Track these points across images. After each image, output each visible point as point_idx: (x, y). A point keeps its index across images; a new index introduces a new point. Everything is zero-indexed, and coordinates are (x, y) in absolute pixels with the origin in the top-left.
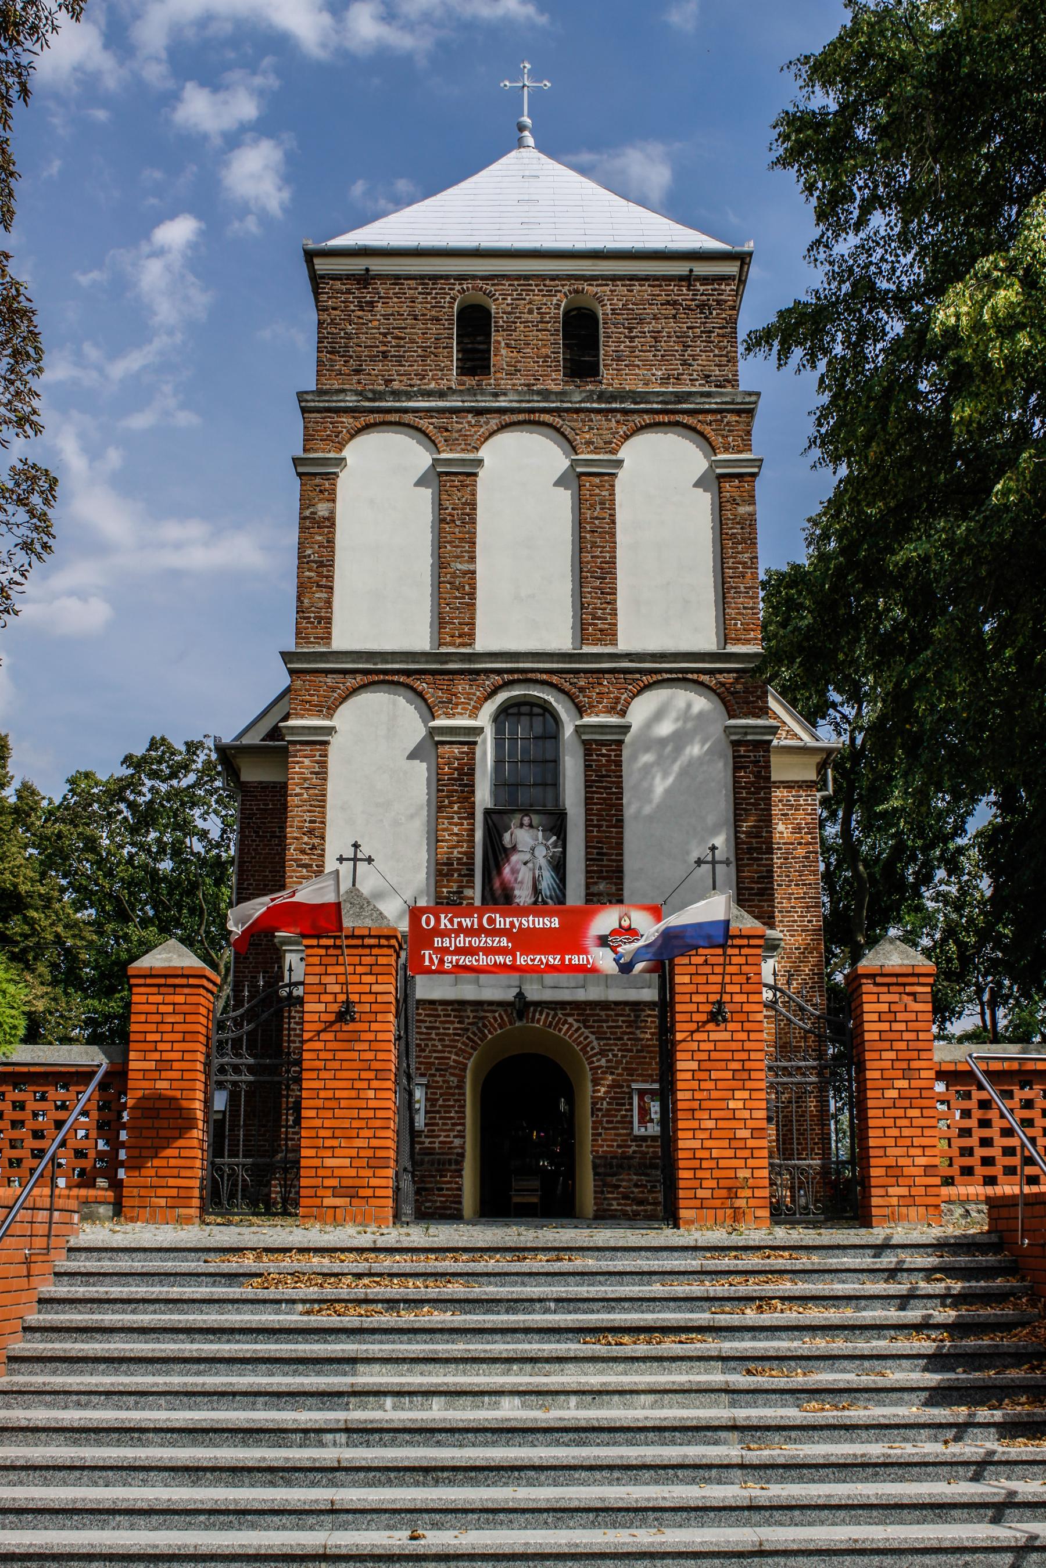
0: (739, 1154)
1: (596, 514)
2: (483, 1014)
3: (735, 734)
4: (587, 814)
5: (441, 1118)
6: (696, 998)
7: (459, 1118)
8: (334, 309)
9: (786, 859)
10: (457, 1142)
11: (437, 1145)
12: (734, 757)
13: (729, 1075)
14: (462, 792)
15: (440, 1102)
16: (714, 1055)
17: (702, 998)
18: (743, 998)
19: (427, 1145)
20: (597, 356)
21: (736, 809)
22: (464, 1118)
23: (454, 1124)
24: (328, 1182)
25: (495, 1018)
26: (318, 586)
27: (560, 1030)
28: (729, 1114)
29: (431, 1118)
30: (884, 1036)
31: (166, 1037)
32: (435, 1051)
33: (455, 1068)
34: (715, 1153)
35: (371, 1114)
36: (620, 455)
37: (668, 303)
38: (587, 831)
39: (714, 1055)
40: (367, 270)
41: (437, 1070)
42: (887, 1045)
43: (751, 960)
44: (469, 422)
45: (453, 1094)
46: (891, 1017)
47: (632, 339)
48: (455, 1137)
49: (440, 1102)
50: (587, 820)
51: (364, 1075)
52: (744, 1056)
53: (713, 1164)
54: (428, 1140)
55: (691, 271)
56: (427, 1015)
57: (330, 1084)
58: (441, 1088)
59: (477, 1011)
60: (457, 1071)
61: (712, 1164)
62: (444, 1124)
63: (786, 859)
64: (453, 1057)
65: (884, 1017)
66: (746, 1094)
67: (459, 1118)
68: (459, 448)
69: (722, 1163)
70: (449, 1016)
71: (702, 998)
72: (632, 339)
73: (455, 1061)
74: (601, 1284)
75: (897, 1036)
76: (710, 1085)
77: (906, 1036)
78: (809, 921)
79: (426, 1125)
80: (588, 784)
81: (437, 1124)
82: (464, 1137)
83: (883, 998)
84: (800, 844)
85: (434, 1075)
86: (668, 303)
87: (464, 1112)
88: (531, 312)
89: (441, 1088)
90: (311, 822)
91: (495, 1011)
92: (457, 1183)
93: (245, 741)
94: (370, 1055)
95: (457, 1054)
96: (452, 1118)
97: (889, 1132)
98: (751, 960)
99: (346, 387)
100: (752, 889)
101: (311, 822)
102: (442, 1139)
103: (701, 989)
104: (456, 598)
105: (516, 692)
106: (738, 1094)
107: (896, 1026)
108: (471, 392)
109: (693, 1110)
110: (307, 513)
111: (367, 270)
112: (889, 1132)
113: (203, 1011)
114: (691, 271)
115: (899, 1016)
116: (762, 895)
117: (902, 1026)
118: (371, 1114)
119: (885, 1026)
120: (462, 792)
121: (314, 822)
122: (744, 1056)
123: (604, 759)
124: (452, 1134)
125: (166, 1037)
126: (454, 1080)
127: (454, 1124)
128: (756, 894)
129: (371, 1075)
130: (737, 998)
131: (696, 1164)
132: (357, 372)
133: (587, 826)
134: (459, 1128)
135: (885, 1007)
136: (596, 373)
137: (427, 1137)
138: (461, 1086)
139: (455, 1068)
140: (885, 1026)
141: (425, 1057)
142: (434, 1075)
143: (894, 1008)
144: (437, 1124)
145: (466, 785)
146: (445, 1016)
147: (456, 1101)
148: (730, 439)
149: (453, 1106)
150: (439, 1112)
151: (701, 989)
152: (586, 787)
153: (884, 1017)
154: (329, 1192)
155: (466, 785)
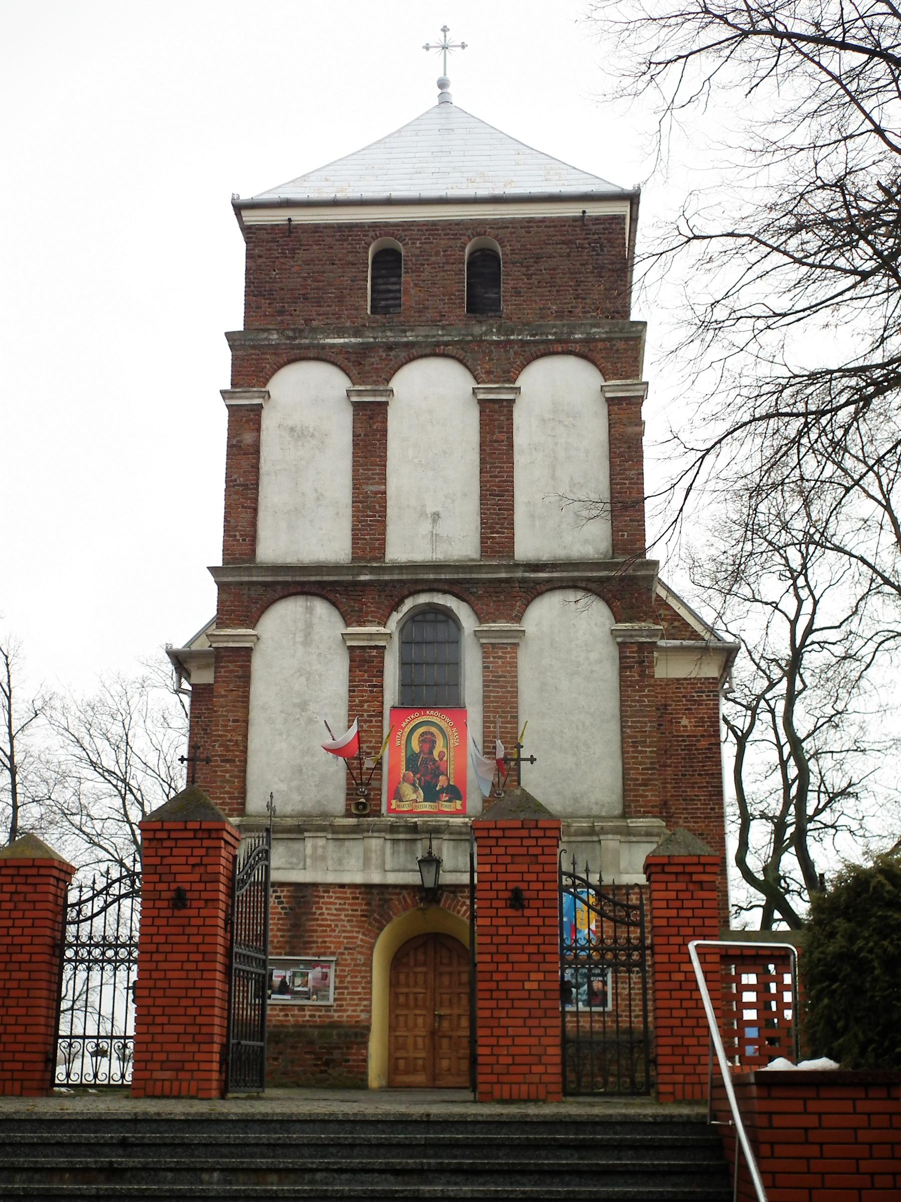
0: (534, 1032)
1: (495, 437)
2: (388, 896)
3: (620, 636)
4: (484, 712)
5: (349, 994)
6: (495, 886)
7: (365, 994)
8: (260, 257)
9: (690, 750)
10: (363, 1016)
11: (317, 1019)
12: (621, 658)
13: (525, 958)
14: (372, 692)
15: (348, 979)
16: (511, 939)
17: (502, 886)
18: (539, 886)
19: (336, 1019)
20: (499, 293)
21: (621, 706)
22: (370, 993)
23: (360, 999)
24: (157, 1057)
25: (399, 900)
26: (243, 507)
27: (459, 912)
28: (525, 995)
29: (340, 994)
30: (672, 922)
31: (17, 923)
32: (344, 931)
33: (362, 947)
34: (511, 1031)
35: (197, 993)
36: (517, 385)
37: (563, 243)
38: (484, 727)
39: (511, 939)
40: (290, 220)
41: (346, 949)
42: (674, 931)
43: (547, 850)
44: (380, 356)
45: (360, 972)
46: (678, 904)
47: (529, 276)
48: (362, 1011)
49: (348, 979)
50: (484, 717)
51: (193, 957)
52: (540, 940)
53: (509, 1041)
54: (336, 1014)
55: (584, 212)
56: (337, 898)
57: (162, 966)
58: (349, 965)
59: (382, 893)
60: (363, 950)
61: (509, 1041)
62: (352, 999)
63: (690, 750)
64: (361, 936)
65: (671, 904)
66: (540, 976)
67: (365, 994)
68: (371, 380)
69: (518, 1041)
70: (357, 898)
71: (502, 886)
72: (529, 276)
73: (362, 940)
74: (333, 1155)
75: (684, 922)
76: (507, 967)
77: (693, 922)
78: (712, 809)
79: (335, 1000)
80: (486, 684)
81: (345, 999)
82: (370, 1011)
83: (670, 886)
84: (703, 736)
85: (343, 954)
86: (563, 243)
87: (371, 989)
88: (437, 254)
89: (349, 965)
90: (234, 721)
91: (399, 894)
92: (362, 1055)
93: (194, 647)
94: (199, 939)
95: (364, 934)
96: (359, 994)
97: (675, 1013)
98: (547, 850)
99: (270, 327)
100: (637, 779)
101: (234, 721)
102: (349, 1013)
103: (501, 877)
104: (368, 516)
105: (423, 599)
106: (533, 976)
107: (683, 913)
108: (384, 328)
109: (492, 991)
110: (234, 442)
111: (290, 220)
112: (675, 1013)
113: (51, 898)
114: (584, 212)
115: (686, 904)
116: (646, 785)
117: (689, 913)
118: (197, 993)
119: (673, 913)
120: (372, 692)
121: (237, 721)
122: (540, 940)
123: (500, 661)
124: (359, 1008)
125: (17, 923)
126: (361, 958)
127: (360, 999)
128: (640, 785)
129: (199, 957)
130: (534, 886)
131: (493, 1041)
132: (281, 312)
133: (484, 722)
134: (365, 1003)
135: (673, 895)
136: (498, 309)
137: (335, 1011)
138: (369, 964)
139: (362, 947)
140: (673, 913)
141: (335, 937)
142: (343, 954)
143: (682, 895)
144: (345, 999)
145: (375, 686)
146: (353, 898)
147: (363, 977)
148: (619, 365)
149: (360, 982)
150: (346, 988)
151: (501, 877)
152: (484, 686)
153: (671, 904)
154: (158, 1066)
155: (375, 686)
